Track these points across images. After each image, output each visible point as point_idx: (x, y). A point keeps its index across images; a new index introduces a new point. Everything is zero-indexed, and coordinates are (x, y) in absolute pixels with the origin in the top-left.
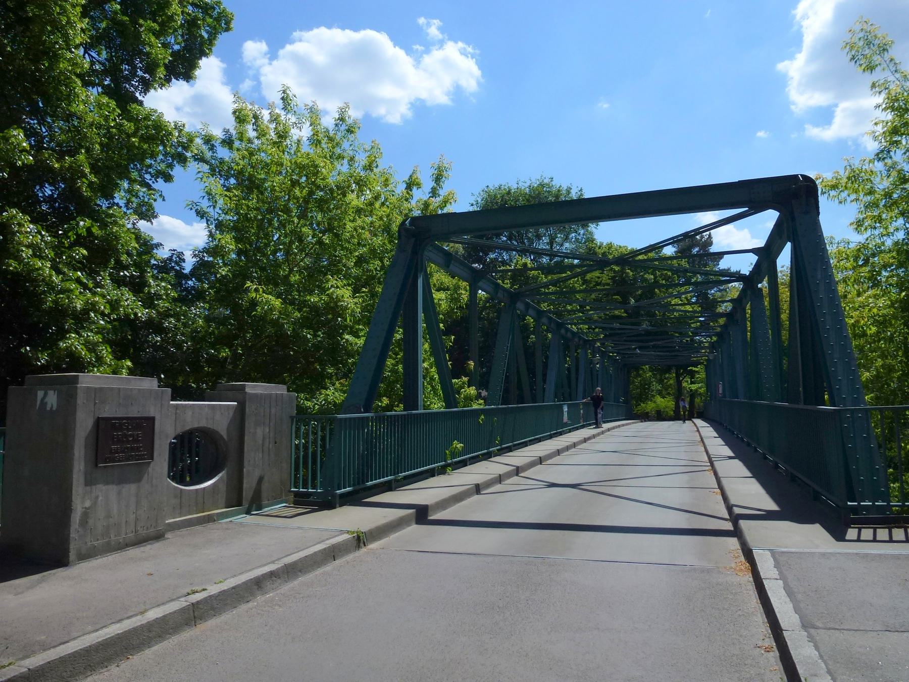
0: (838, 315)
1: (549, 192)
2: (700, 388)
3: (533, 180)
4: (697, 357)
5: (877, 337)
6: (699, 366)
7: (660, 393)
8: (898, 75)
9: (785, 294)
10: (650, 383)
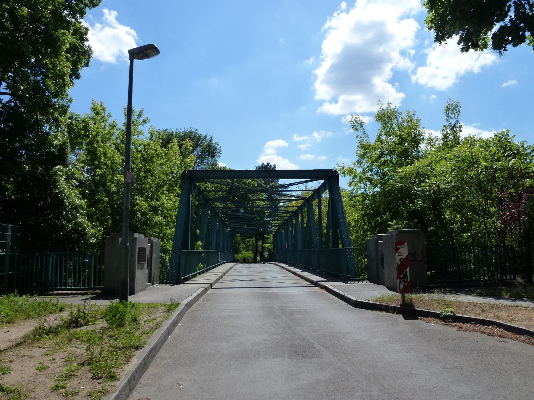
0: (345, 218)
1: (194, 136)
2: (270, 246)
3: (186, 129)
4: (270, 230)
5: (355, 226)
6: (270, 235)
7: (244, 249)
8: (365, 135)
9: (324, 209)
10: (239, 244)
